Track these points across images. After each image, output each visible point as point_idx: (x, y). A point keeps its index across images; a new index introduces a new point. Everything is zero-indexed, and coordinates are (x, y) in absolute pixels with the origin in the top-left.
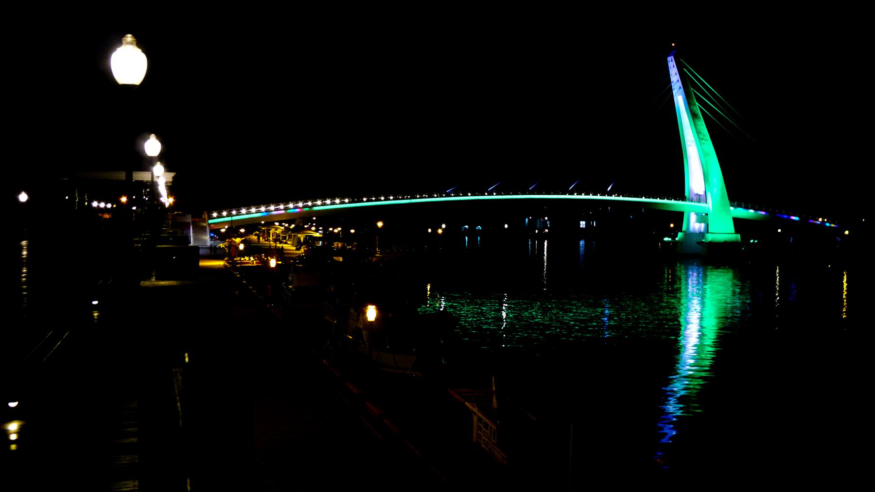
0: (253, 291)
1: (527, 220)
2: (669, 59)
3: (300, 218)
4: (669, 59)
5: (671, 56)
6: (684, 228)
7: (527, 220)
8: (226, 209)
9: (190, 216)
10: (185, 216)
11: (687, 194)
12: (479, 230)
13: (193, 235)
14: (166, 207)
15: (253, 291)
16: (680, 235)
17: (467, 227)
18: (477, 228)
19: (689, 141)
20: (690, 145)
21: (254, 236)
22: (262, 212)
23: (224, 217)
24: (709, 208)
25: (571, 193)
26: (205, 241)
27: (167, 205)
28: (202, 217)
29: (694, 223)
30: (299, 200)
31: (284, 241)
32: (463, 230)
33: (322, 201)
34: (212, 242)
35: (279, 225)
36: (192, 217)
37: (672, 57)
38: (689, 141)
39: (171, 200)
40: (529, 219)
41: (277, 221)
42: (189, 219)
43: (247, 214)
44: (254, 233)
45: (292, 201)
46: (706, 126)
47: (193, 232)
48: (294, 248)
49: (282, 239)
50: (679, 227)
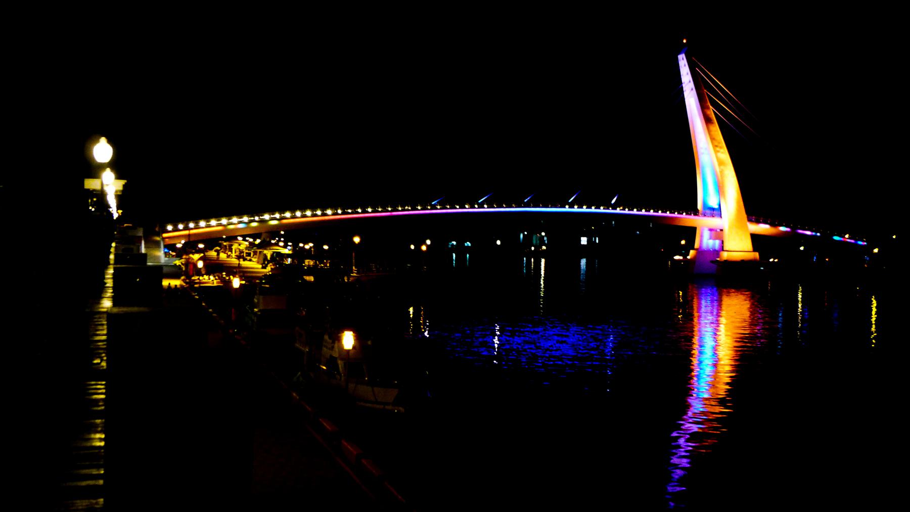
1: (522, 236)
3: (266, 232)
6: (697, 246)
7: (522, 236)
12: (468, 246)
18: (466, 245)
19: (702, 148)
26: (158, 258)
31: (248, 258)
32: (450, 246)
34: (166, 259)
40: (524, 235)
49: (246, 256)
50: (691, 245)
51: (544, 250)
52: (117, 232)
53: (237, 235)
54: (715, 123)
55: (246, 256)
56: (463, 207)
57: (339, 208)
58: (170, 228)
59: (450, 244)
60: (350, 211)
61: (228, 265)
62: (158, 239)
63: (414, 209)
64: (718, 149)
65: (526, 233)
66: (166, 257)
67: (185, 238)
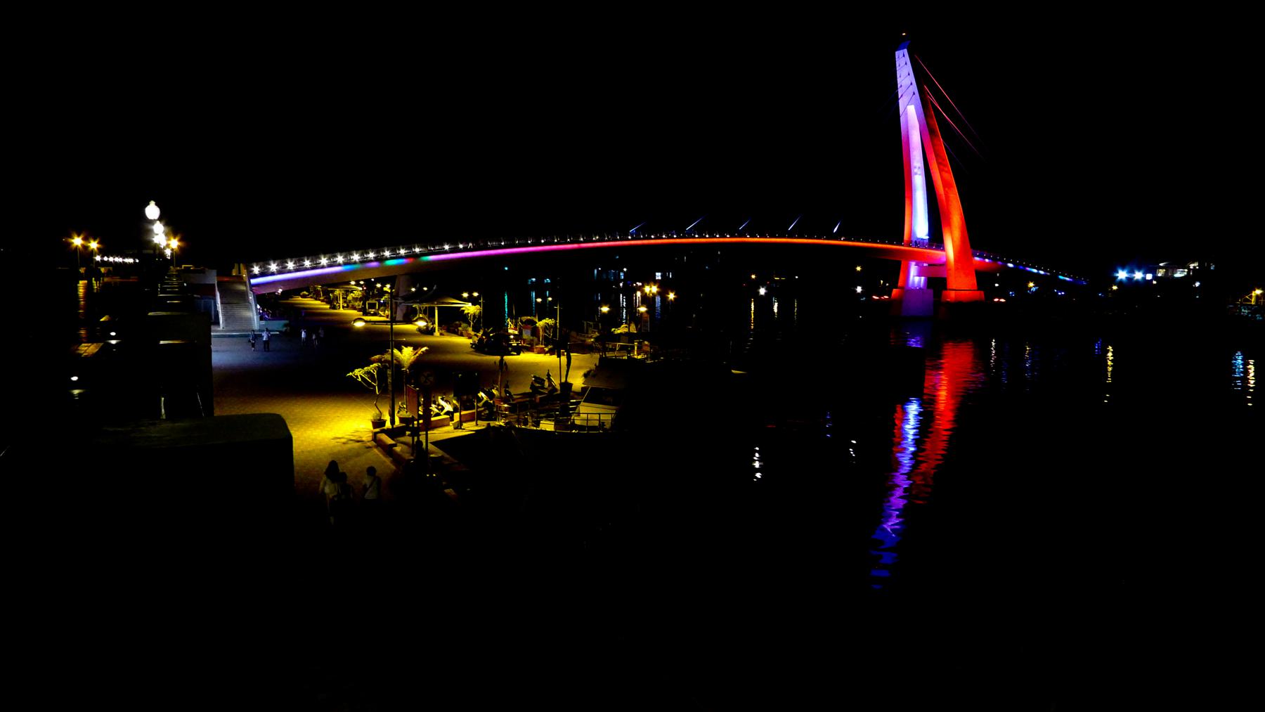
0: (447, 491)
1: (596, 271)
2: (899, 54)
3: (406, 274)
4: (899, 54)
5: (903, 49)
6: (900, 284)
7: (596, 271)
8: (257, 262)
9: (214, 272)
10: (203, 272)
11: (906, 237)
12: (547, 283)
13: (223, 309)
14: (152, 203)
15: (447, 491)
16: (895, 291)
17: (534, 279)
18: (545, 281)
19: (915, 167)
20: (916, 174)
21: (300, 298)
22: (339, 265)
23: (306, 269)
24: (947, 257)
25: (742, 235)
26: (249, 320)
27: (168, 252)
28: (231, 272)
29: (914, 276)
30: (304, 256)
31: (372, 311)
32: (529, 283)
33: (329, 259)
34: (263, 322)
35: (355, 285)
36: (218, 275)
37: (906, 50)
38: (915, 167)
39: (175, 243)
40: (598, 270)
41: (362, 280)
42: (213, 278)
43: (330, 266)
44: (302, 294)
45: (341, 252)
46: (902, 158)
47: (222, 303)
48: (328, 306)
49: (369, 308)
50: (894, 284)
51: (86, 271)
52: (597, 311)
53: (359, 279)
54: (937, 136)
55: (369, 308)
56: (712, 236)
57: (386, 249)
58: (256, 270)
59: (530, 281)
60: (447, 247)
61: (326, 318)
62: (243, 288)
63: (537, 244)
64: (942, 167)
65: (625, 270)
66: (534, 377)
67: (283, 285)
